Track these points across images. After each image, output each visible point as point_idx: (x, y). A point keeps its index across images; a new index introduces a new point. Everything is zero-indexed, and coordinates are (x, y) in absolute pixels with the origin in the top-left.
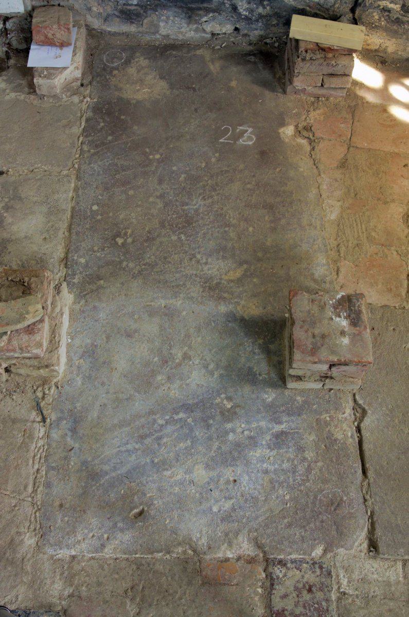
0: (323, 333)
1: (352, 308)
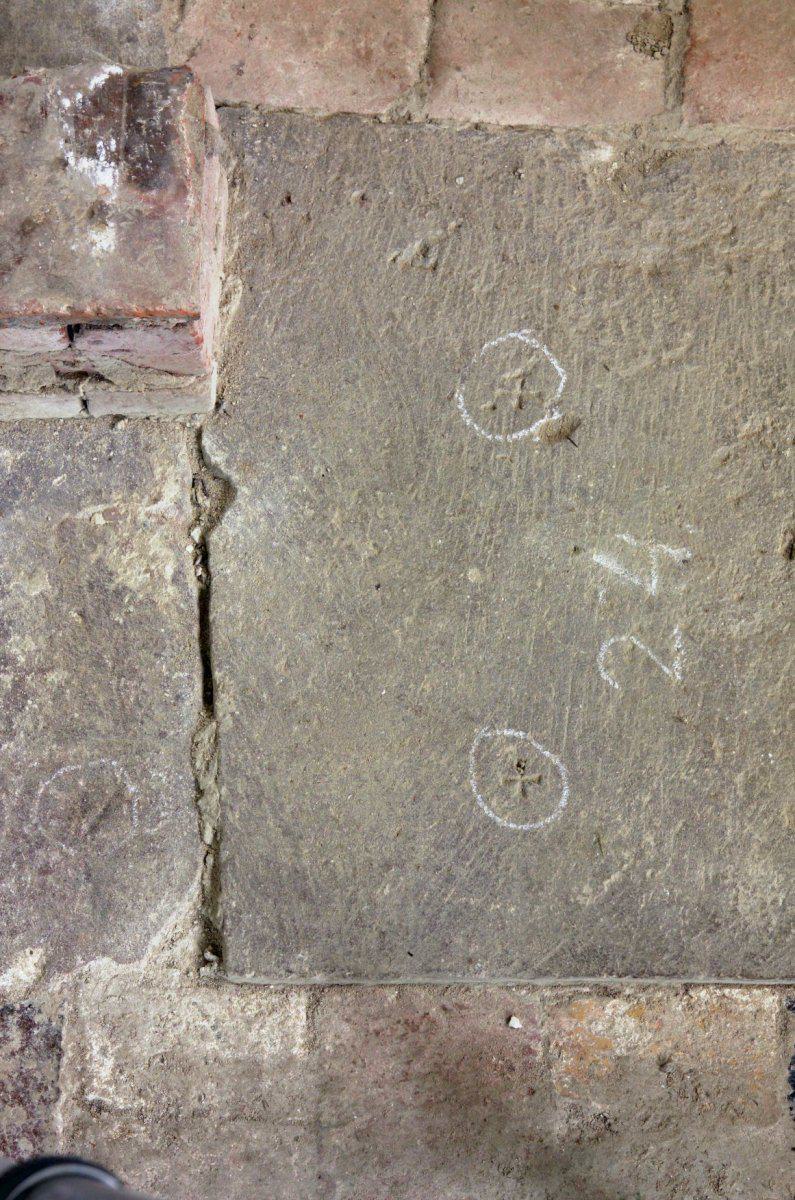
1: (140, 121)
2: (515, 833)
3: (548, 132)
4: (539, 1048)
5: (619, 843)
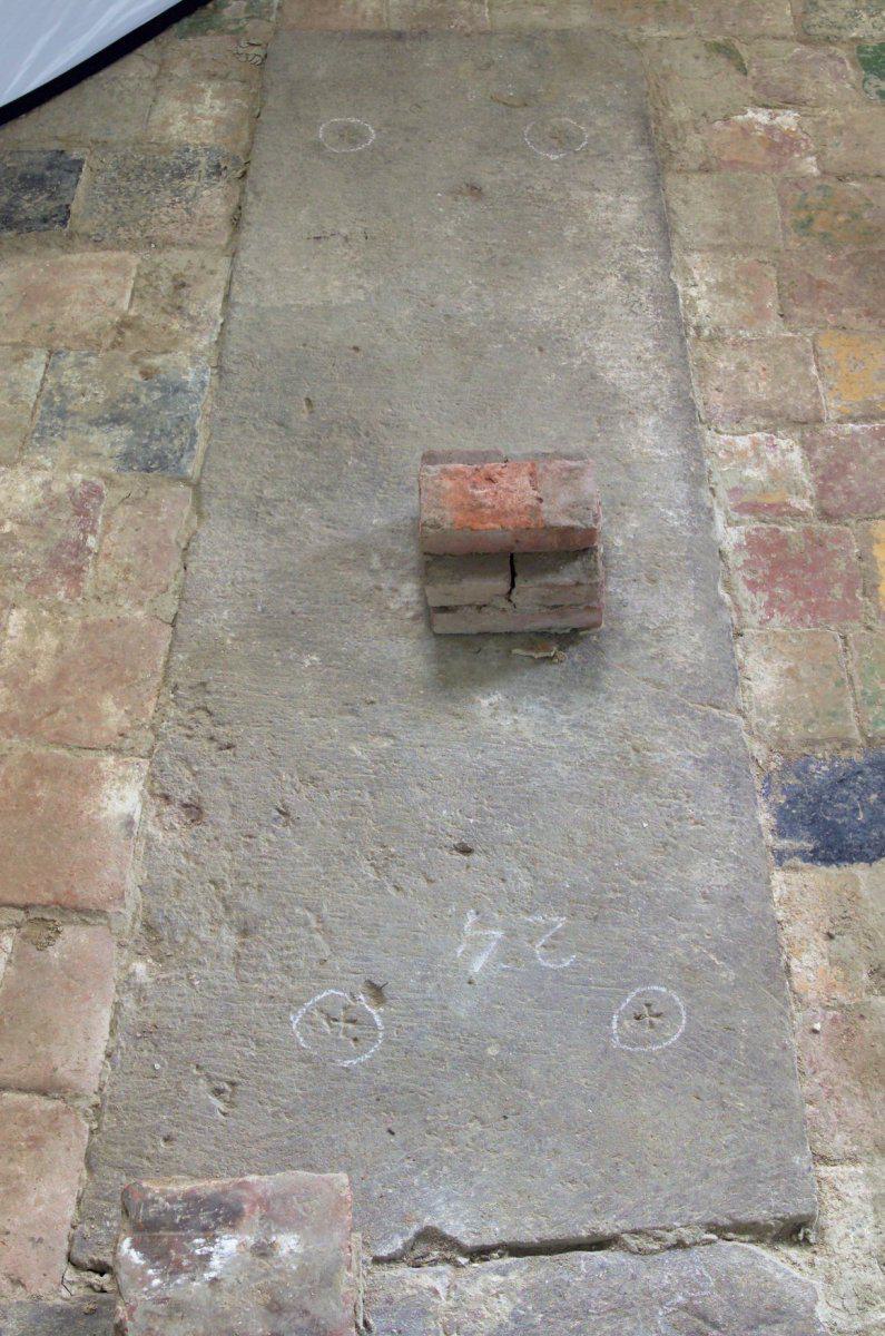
0: (263, 1309)
1: (177, 1221)
2: (689, 1020)
3: (118, 1006)
4: (831, 1014)
5: (688, 954)
